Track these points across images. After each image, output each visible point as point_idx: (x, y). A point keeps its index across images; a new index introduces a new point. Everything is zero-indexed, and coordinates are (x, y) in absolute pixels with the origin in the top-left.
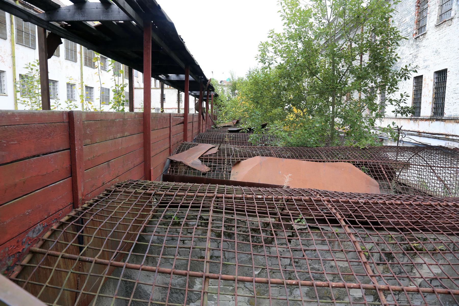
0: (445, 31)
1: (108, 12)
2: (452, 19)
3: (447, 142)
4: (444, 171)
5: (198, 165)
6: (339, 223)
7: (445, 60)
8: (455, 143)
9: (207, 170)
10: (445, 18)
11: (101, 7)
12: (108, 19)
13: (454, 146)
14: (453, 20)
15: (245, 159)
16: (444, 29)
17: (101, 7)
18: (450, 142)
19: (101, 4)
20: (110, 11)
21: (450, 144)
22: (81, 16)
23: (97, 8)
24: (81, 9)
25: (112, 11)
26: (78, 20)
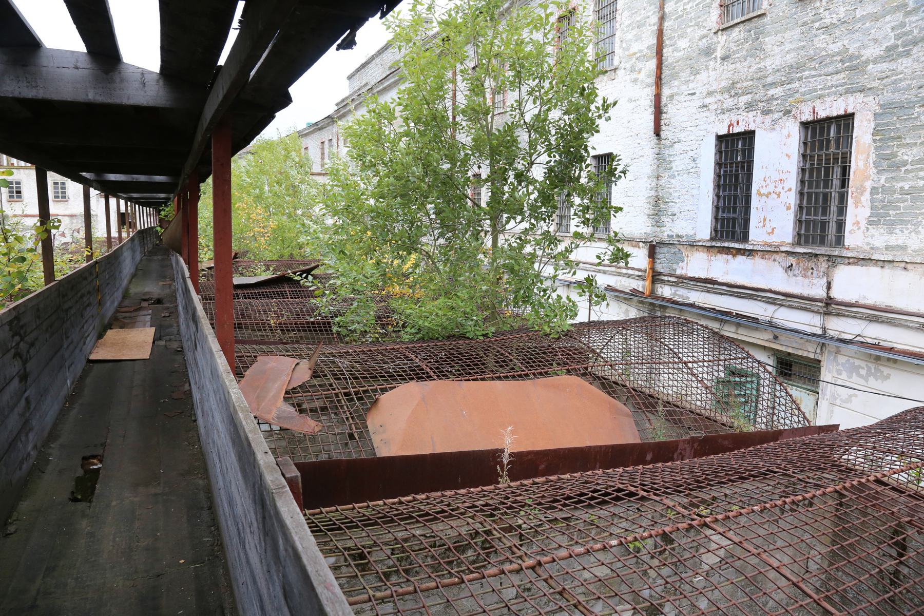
0: (606, 87)
1: (112, 81)
2: (616, 69)
3: (619, 278)
4: (715, 368)
5: (292, 418)
6: (638, 495)
7: (608, 138)
8: (631, 280)
9: (317, 430)
10: (605, 65)
11: (89, 66)
12: (109, 101)
13: (630, 287)
14: (618, 72)
15: (391, 388)
16: (604, 84)
17: (89, 66)
18: (623, 279)
19: (85, 62)
20: (118, 80)
21: (623, 283)
22: (25, 84)
23: (77, 68)
24: (25, 65)
25: (122, 80)
26: (16, 94)
